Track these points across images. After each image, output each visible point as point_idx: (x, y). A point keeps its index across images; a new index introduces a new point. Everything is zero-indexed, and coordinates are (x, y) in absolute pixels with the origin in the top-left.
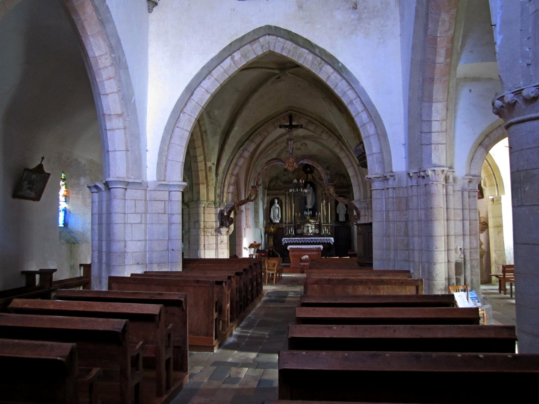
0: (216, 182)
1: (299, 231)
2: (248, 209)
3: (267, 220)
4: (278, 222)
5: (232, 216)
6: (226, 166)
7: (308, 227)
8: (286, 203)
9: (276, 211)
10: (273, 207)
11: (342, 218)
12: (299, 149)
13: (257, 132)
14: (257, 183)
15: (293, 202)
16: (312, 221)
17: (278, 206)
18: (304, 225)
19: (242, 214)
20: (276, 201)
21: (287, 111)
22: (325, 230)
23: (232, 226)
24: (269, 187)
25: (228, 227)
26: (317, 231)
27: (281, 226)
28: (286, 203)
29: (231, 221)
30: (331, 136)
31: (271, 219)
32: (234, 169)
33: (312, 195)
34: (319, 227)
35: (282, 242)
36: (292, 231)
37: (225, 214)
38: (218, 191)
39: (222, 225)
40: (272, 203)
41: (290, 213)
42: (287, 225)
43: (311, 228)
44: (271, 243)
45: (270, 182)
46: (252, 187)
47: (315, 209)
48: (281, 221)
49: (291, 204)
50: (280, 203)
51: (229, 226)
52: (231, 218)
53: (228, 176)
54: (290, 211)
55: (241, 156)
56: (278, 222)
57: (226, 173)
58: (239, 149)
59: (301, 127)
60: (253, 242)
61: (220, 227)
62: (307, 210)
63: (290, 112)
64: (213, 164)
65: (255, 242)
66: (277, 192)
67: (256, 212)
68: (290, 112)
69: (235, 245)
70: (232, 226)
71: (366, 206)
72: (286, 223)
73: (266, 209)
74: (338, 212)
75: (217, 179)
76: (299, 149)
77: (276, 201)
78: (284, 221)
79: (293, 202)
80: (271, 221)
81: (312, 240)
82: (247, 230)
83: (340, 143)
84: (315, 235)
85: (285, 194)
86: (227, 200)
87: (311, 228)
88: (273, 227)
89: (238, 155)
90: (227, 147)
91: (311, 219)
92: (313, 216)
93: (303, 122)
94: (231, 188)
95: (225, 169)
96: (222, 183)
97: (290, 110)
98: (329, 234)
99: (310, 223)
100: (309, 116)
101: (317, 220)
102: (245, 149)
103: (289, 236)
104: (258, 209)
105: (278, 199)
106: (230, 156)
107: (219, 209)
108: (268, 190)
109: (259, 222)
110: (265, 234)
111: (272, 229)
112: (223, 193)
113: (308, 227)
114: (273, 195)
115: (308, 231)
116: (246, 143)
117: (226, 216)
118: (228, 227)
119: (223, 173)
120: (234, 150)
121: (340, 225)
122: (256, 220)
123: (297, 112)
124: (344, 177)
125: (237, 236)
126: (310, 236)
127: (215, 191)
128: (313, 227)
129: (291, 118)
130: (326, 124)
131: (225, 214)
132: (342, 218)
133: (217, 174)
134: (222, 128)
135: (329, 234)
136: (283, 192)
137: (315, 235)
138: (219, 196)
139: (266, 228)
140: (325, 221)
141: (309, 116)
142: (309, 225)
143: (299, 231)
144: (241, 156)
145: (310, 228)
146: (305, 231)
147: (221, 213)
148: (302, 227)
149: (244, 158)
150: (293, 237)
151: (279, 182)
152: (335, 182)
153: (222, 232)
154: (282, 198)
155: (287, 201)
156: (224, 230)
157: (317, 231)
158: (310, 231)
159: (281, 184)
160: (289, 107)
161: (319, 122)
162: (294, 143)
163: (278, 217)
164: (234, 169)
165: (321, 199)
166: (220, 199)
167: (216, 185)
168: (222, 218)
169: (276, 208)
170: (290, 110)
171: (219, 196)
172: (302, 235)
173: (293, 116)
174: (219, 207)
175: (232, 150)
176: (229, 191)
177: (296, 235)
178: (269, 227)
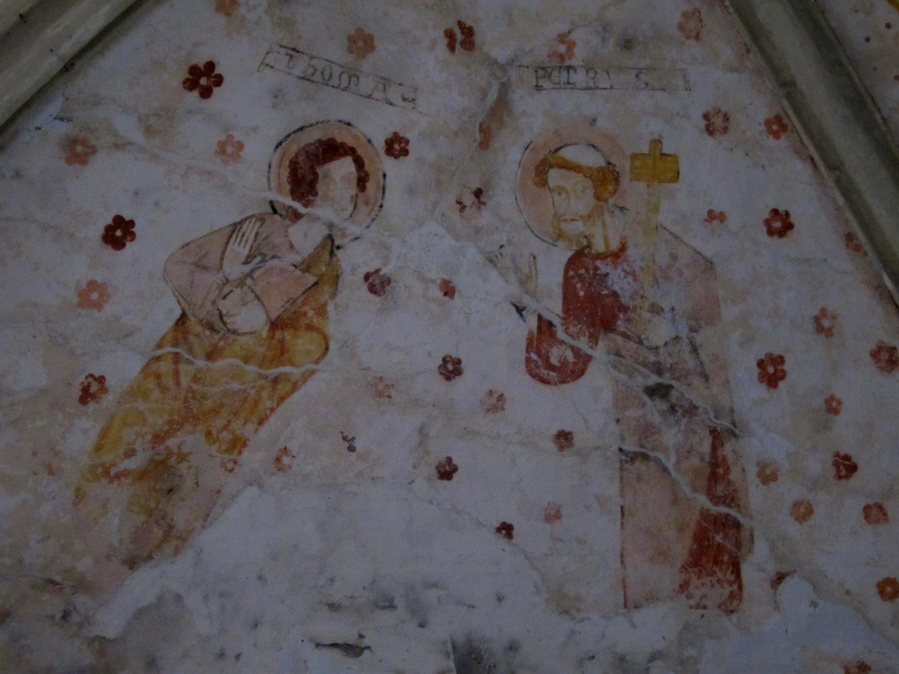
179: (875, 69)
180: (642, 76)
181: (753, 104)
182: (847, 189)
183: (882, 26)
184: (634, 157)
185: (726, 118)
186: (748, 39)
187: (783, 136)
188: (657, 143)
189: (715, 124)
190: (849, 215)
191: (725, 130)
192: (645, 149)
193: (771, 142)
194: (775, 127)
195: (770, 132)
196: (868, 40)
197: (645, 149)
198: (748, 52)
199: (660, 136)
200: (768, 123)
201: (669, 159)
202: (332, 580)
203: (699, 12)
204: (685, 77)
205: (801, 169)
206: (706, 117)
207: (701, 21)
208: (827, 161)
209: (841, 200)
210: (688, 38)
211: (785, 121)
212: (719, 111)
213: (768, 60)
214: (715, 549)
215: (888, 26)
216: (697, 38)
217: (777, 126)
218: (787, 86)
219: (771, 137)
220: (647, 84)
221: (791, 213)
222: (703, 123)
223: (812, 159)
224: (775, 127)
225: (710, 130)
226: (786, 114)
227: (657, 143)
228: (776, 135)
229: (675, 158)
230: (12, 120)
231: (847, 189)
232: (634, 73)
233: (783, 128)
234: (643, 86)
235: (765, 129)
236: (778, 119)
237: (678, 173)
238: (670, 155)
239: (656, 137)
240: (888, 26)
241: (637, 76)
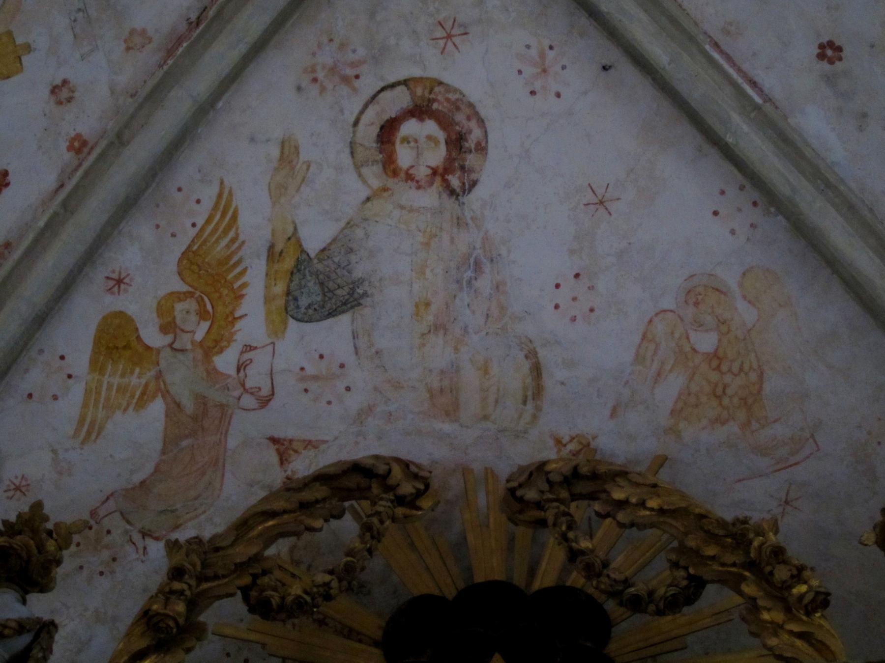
179: (158, 206)
180: (81, 14)
181: (89, 117)
182: (52, 228)
183: (195, 197)
184: (10, 34)
185: (69, 100)
186: (143, 93)
187: (72, 154)
188: (28, 48)
189: (62, 93)
190: (31, 236)
191: (60, 103)
192: (20, 40)
193: (64, 145)
194: (76, 144)
195: (72, 140)
196: (180, 190)
197: (20, 40)
198: (132, 96)
199: (35, 49)
200: (78, 137)
201: (18, 65)
202: (357, 77)
203: (150, 43)
204: (92, 51)
205: (50, 180)
206: (65, 82)
207: (143, 47)
208: (67, 201)
209: (41, 224)
210: (125, 41)
211: (86, 150)
212: (73, 92)
213: (133, 117)
215: (198, 201)
216: (128, 49)
217: (79, 145)
218: (120, 140)
219: (68, 144)
220: (75, 21)
221: (10, 186)
222: (58, 81)
223: (62, 186)
224: (76, 144)
225: (54, 90)
226: (92, 148)
227: (28, 48)
228: (70, 148)
229: (20, 70)
230: (594, 14)
231: (52, 228)
232: (81, 6)
233: (78, 151)
234: (73, 19)
235: (73, 135)
236: (84, 143)
237: (8, 77)
238: (21, 64)
239: (33, 46)
240: (198, 201)
241: (79, 10)
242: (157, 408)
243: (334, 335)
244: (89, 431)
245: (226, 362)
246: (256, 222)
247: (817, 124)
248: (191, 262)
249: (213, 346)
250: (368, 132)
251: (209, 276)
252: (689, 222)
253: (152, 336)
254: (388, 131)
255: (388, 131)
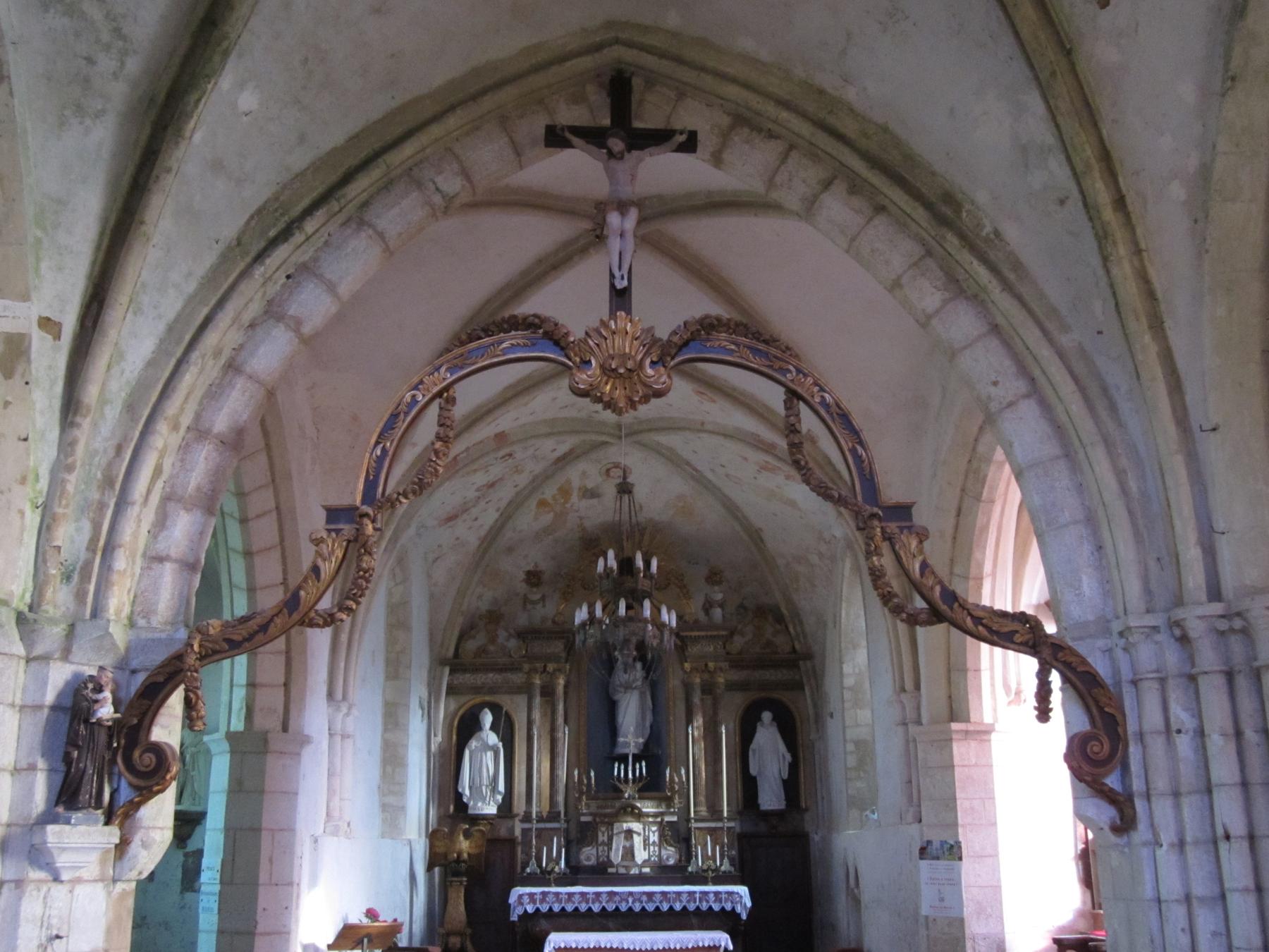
0: (62, 466)
1: (588, 855)
2: (345, 736)
3: (441, 804)
4: (491, 809)
5: (168, 729)
6: (151, 364)
7: (629, 833)
8: (530, 723)
9: (484, 763)
10: (473, 744)
11: (771, 798)
12: (591, 494)
13: (397, 158)
14: (370, 485)
15: (560, 720)
16: (648, 807)
17: (492, 739)
18: (611, 825)
19: (307, 753)
20: (488, 718)
21: (598, 48)
22: (707, 852)
23: (159, 814)
24: (456, 655)
25: (120, 815)
26: (670, 855)
27: (503, 832)
28: (530, 723)
29: (151, 772)
30: (880, 209)
31: (459, 796)
32: (214, 394)
33: (642, 694)
34: (678, 835)
35: (507, 908)
36: (554, 854)
37: (106, 712)
38: (72, 536)
39: (68, 796)
40: (466, 728)
41: (548, 771)
42: (535, 825)
43: (641, 841)
44: (458, 910)
45: (462, 638)
46: (334, 514)
47: (654, 754)
48: (506, 808)
49: (553, 730)
50: (505, 728)
51: (135, 806)
52: (158, 750)
53: (164, 438)
54: (546, 765)
55: (273, 312)
56: (491, 809)
57: (147, 409)
58: (260, 257)
59: (690, 145)
60: (357, 917)
61: (49, 818)
62: (623, 759)
63: (618, 52)
64: (48, 325)
65: (371, 914)
66: (491, 677)
67: (392, 759)
68: (618, 52)
69: (251, 934)
70: (159, 814)
71: (1173, 658)
72: (527, 818)
73: (442, 753)
74: (753, 771)
75: (66, 446)
76: (591, 494)
77: (488, 718)
78: (519, 806)
79: (560, 720)
80: (461, 806)
81: (650, 895)
82: (331, 845)
83: (952, 241)
84: (663, 873)
85: (526, 689)
86: (140, 608)
87: (641, 841)
88: (467, 835)
89: (249, 300)
90: (162, 216)
91: (641, 798)
92: (652, 786)
93: (690, 117)
94: (183, 529)
95: (140, 387)
96: (108, 482)
97: (617, 41)
98: (726, 867)
99: (639, 816)
100: (734, 80)
101: (669, 801)
102: (303, 271)
103: (542, 878)
104: (406, 746)
105: (496, 709)
106: (192, 301)
107: (59, 676)
108: (452, 672)
109: (403, 809)
110: (430, 868)
111: (464, 845)
112: (109, 549)
113: (629, 833)
114: (477, 690)
115: (629, 853)
116: (310, 226)
117: (115, 729)
118: (120, 815)
119: (130, 408)
120: (225, 258)
121: (763, 827)
122: (391, 800)
123: (663, 55)
124: (780, 619)
125: (263, 877)
126: (641, 879)
127: (46, 529)
128: (654, 838)
129: (619, 88)
130: (849, 127)
131: (106, 712)
132: (771, 798)
133: (71, 406)
134: (133, 65)
135: (726, 867)
136: (517, 678)
137: (663, 873)
138: (77, 574)
139: (433, 836)
140: (703, 810)
141: (734, 80)
142: (636, 826)
143: (588, 855)
144: (273, 312)
145: (638, 841)
146: (616, 856)
147: (75, 706)
148: (602, 838)
149: (297, 325)
150: (563, 880)
151: (502, 634)
152: (738, 642)
153: (62, 860)
154: (517, 707)
155: (537, 715)
156: (81, 841)
157: (670, 855)
158: (641, 855)
159: (513, 643)
160: (609, 25)
161: (804, 115)
162: (641, 221)
163: (494, 790)
164: (214, 394)
165: (681, 707)
166: (80, 596)
167: (56, 483)
168: (72, 742)
169: (487, 747)
170: (617, 41)
171: (77, 574)
172: (601, 873)
173: (637, 82)
174: (66, 654)
175: (209, 259)
176: (161, 547)
177: (575, 874)
178: (452, 835)
214: (451, 518)
242: (552, 514)
243: (595, 501)
244: (536, 519)
245: (568, 506)
246: (576, 483)
247: (710, 476)
248: (560, 489)
249: (566, 502)
250: (604, 469)
251: (565, 492)
252: (678, 486)
253: (550, 501)
254: (608, 470)
255: (608, 470)
